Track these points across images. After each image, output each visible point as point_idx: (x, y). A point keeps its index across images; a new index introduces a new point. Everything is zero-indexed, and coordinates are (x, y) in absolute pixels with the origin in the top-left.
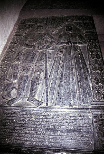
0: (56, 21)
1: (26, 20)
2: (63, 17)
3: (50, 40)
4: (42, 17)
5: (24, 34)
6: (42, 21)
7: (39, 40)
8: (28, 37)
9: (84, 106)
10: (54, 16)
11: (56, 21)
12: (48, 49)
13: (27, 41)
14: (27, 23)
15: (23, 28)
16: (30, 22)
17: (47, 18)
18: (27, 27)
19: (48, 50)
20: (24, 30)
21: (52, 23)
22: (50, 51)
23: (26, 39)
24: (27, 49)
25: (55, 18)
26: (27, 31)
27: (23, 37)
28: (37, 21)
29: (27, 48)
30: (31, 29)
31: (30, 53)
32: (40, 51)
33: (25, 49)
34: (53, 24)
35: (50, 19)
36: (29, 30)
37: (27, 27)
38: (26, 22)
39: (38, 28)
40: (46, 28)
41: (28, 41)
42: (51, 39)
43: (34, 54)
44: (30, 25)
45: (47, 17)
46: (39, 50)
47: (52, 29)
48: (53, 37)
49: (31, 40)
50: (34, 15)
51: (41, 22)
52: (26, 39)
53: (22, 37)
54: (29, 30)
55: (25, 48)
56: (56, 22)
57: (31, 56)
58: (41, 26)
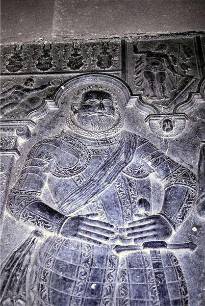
0: (168, 61)
1: (17, 56)
2: (198, 38)
3: (163, 183)
4: (94, 37)
5: (21, 141)
6: (99, 64)
7: (108, 181)
8: (44, 160)
9: (141, 232)
10: (154, 34)
11: (168, 61)
12: (163, 245)
13: (42, 185)
14: (25, 69)
15: (11, 105)
16: (43, 67)
17: (124, 44)
18: (30, 95)
19: (162, 250)
20: (14, 116)
21: (149, 75)
22: (174, 251)
23: (37, 172)
24: (49, 241)
25: (162, 46)
26: (35, 119)
27: (17, 157)
28: (75, 64)
29: (47, 234)
30: (51, 106)
31: (72, 268)
32: (123, 255)
33: (40, 241)
34: (157, 84)
35: (136, 51)
36: (43, 116)
37: (30, 95)
38: (20, 67)
39: (86, 108)
40: (123, 107)
41: (46, 185)
42: (167, 174)
43: (94, 279)
44: (43, 87)
45: (119, 42)
46: (119, 249)
47: (159, 115)
48: (172, 164)
49: (137, 301)
50: (55, 28)
51: (97, 68)
52: (37, 172)
53: (13, 159)
54: (43, 116)
55: (36, 233)
56: (172, 68)
57: (80, 295)
58: (101, 95)
